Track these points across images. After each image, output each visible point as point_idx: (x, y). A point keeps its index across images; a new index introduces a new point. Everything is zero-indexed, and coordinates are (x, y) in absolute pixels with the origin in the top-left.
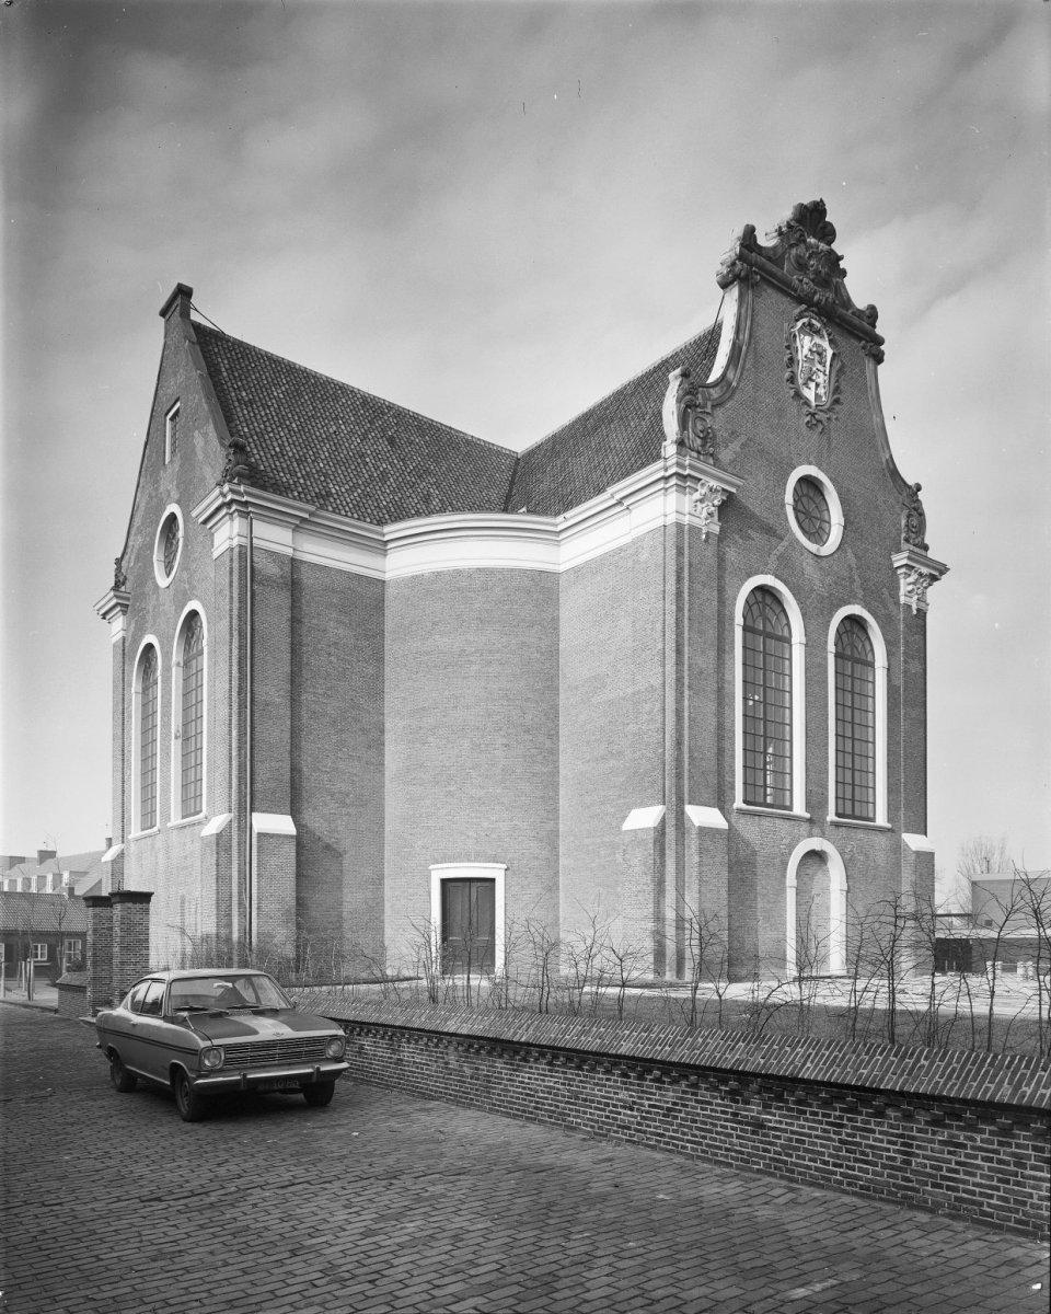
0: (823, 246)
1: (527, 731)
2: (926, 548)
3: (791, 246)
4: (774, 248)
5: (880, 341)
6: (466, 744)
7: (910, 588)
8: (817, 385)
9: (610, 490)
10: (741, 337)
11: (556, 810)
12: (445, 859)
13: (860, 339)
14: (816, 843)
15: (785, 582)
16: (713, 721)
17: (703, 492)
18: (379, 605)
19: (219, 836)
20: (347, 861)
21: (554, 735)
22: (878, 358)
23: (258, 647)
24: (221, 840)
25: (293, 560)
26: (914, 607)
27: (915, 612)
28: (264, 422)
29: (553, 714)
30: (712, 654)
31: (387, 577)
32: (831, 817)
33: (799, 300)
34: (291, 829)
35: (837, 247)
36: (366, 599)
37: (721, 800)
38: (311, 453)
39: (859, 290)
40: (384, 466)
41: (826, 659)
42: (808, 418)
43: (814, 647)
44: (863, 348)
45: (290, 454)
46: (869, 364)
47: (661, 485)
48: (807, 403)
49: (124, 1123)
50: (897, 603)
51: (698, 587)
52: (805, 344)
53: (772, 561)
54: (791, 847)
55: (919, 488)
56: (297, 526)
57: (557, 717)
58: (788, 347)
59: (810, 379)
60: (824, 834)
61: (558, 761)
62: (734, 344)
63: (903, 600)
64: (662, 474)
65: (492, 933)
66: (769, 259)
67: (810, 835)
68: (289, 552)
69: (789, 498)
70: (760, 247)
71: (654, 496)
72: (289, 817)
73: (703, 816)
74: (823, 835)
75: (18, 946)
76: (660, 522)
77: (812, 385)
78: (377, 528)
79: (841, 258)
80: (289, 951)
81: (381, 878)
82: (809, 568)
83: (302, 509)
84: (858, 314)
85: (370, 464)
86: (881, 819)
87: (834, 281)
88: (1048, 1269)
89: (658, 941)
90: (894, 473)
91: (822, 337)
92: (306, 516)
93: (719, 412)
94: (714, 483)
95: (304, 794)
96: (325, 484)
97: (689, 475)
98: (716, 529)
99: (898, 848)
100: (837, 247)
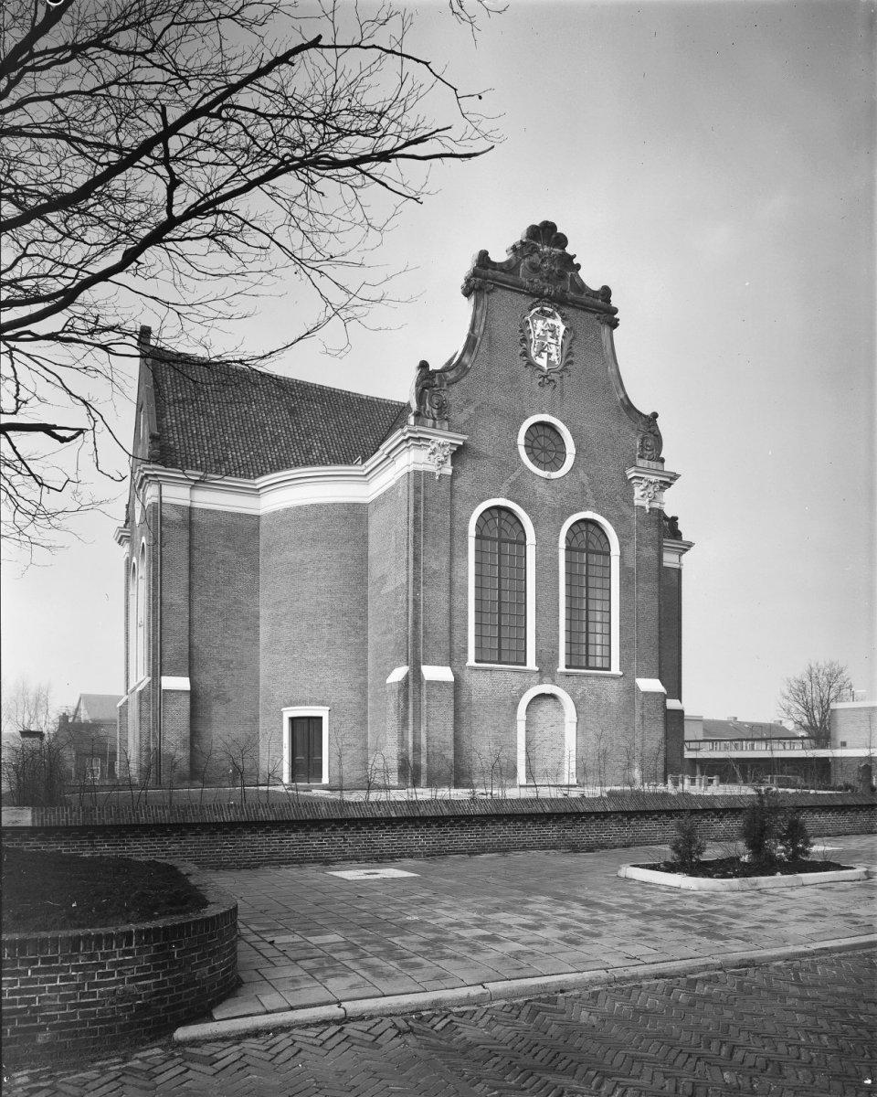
0: (558, 251)
1: (344, 615)
2: (662, 461)
3: (524, 258)
4: (508, 262)
5: (615, 311)
6: (304, 624)
7: (642, 493)
8: (550, 354)
9: (382, 447)
10: (476, 331)
11: (366, 669)
12: (292, 704)
13: (595, 313)
14: (547, 688)
15: (518, 502)
16: (446, 606)
17: (433, 448)
18: (256, 531)
21: (364, 617)
22: (614, 324)
23: (165, 569)
24: (405, 684)
25: (191, 509)
26: (647, 507)
27: (648, 511)
28: (190, 413)
29: (364, 601)
30: (445, 559)
31: (260, 513)
32: (562, 668)
33: (533, 295)
35: (569, 250)
36: (243, 533)
37: (452, 657)
38: (221, 430)
39: (592, 277)
40: (280, 431)
41: (557, 554)
42: (541, 380)
43: (546, 548)
45: (204, 434)
46: (606, 330)
47: (404, 445)
48: (540, 368)
50: (631, 504)
51: (432, 513)
52: (539, 325)
53: (505, 488)
54: (522, 692)
55: (655, 415)
56: (193, 486)
57: (366, 604)
58: (521, 331)
59: (543, 351)
60: (554, 681)
61: (366, 634)
62: (469, 337)
64: (402, 438)
66: (503, 270)
67: (541, 682)
68: (188, 503)
69: (521, 440)
70: (495, 264)
72: (449, 668)
73: (436, 673)
74: (553, 682)
76: (405, 471)
77: (545, 355)
78: (252, 481)
83: (195, 475)
84: (595, 294)
85: (268, 432)
86: (616, 669)
87: (569, 274)
89: (402, 760)
90: (629, 407)
91: (555, 318)
93: (455, 388)
94: (442, 440)
96: (224, 452)
97: (410, 438)
98: (448, 470)
99: (633, 689)
100: (569, 250)
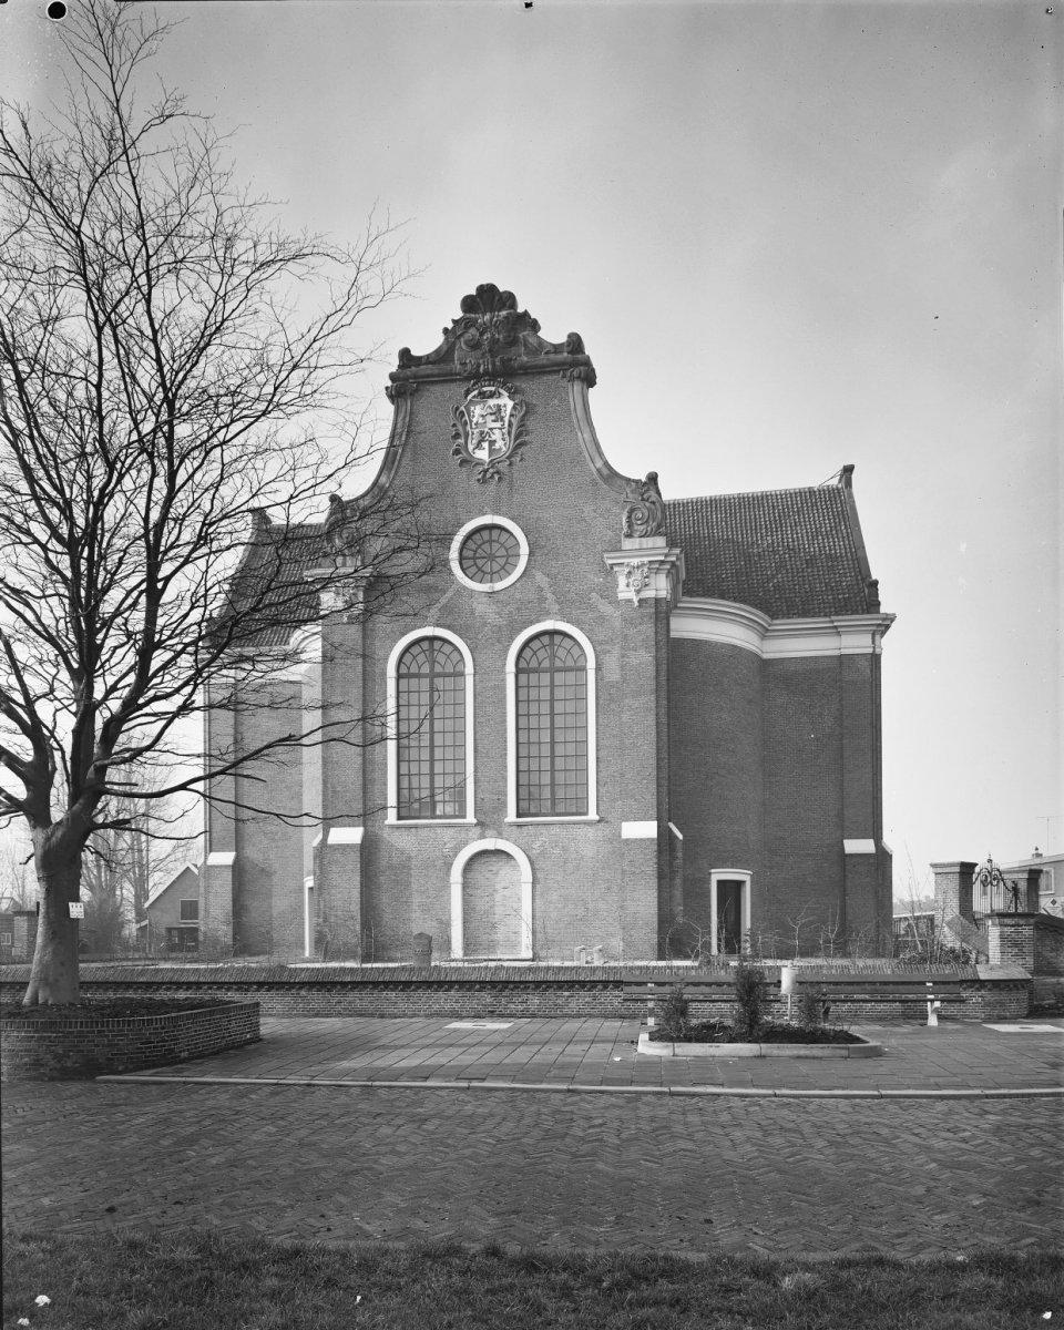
20: (275, 879)
27: (636, 604)
41: (504, 680)
44: (564, 377)
54: (456, 851)
63: (621, 596)
80: (229, 940)
82: (482, 608)
88: (4, 1161)
92: (662, 558)
95: (247, 837)
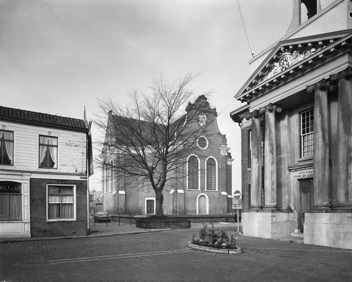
2: (227, 145)
14: (203, 194)
19: (114, 194)
26: (224, 155)
32: (206, 190)
34: (124, 193)
37: (184, 188)
49: (172, 122)
54: (197, 195)
55: (225, 135)
65: (154, 208)
67: (201, 193)
71: (260, 58)
74: (204, 193)
75: (1, 239)
79: (208, 102)
81: (138, 200)
86: (217, 190)
100: (207, 101)
